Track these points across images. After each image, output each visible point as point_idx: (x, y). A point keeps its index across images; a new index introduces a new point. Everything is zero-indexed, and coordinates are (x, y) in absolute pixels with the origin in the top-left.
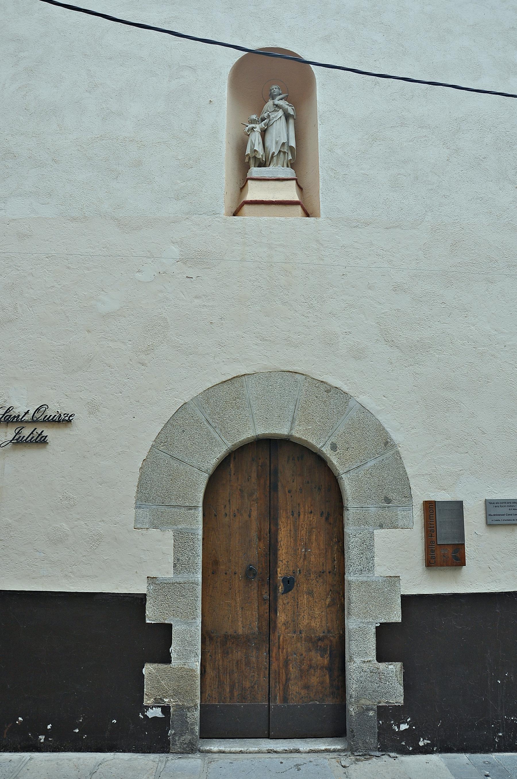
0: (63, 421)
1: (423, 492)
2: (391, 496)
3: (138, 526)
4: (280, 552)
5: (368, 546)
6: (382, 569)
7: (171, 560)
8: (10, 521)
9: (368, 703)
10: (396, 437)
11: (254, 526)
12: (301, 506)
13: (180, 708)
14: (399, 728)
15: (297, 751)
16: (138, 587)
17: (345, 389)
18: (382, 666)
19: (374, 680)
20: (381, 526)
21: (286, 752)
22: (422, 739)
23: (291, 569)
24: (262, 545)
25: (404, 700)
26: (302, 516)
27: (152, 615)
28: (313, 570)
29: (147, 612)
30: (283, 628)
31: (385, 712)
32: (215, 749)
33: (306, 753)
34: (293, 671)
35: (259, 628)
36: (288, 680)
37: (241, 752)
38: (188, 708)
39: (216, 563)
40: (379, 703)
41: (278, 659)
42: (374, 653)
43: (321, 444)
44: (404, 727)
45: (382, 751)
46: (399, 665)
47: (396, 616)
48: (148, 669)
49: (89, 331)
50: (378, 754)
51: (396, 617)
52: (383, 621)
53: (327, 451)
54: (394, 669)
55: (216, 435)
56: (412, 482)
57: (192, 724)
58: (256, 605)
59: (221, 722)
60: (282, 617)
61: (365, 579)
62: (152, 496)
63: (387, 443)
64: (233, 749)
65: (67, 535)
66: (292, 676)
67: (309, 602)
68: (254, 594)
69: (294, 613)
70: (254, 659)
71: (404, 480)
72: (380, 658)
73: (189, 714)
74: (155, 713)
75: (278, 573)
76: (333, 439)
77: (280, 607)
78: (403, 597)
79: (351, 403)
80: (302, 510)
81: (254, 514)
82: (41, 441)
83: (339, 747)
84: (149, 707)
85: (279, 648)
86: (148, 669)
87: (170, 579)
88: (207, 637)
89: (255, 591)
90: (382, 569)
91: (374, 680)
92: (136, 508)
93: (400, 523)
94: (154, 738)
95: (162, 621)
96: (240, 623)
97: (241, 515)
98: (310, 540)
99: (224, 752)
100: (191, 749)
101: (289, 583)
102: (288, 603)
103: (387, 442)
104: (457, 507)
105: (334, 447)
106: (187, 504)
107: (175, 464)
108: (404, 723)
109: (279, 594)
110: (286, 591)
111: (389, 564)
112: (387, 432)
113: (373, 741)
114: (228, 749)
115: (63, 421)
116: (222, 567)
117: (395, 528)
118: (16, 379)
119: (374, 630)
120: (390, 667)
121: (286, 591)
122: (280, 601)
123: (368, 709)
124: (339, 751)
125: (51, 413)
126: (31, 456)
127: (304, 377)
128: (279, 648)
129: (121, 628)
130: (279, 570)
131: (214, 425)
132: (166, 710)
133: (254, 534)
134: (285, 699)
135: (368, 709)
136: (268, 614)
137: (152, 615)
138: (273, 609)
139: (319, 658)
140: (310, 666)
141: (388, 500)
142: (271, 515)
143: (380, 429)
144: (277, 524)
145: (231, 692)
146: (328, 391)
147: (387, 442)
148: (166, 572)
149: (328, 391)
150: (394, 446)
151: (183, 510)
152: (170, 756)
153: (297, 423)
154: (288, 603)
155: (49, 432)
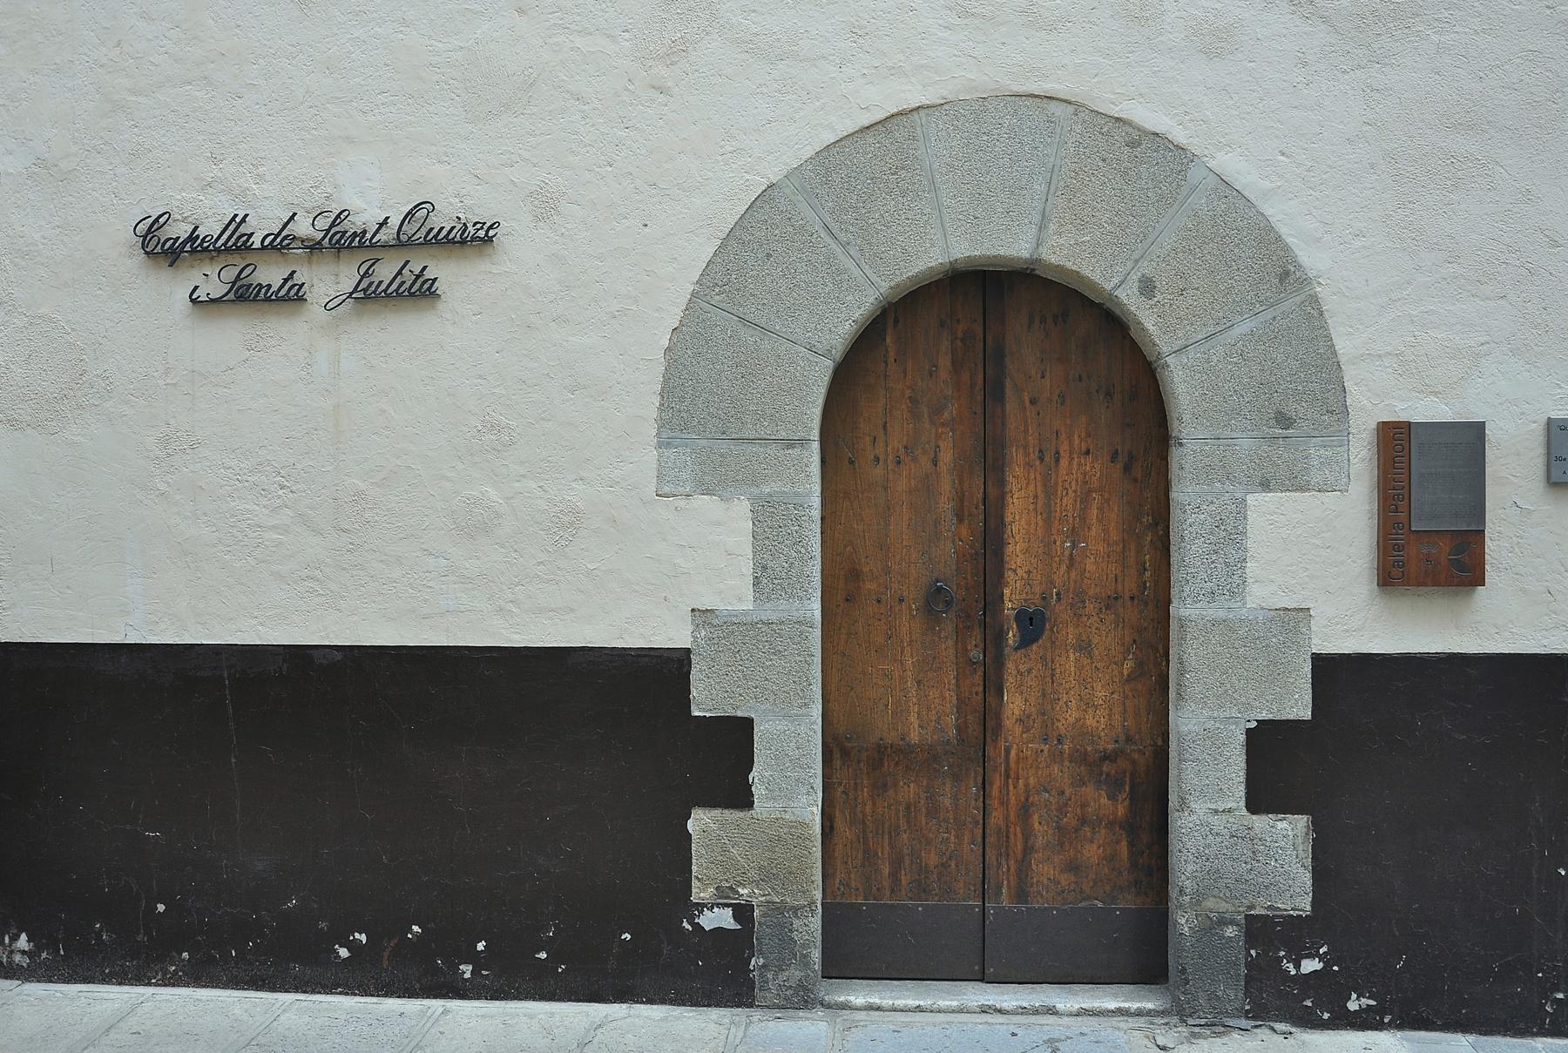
0: (472, 240)
1: (1377, 396)
2: (1291, 409)
3: (667, 489)
4: (1009, 549)
5: (1232, 534)
6: (1265, 590)
7: (747, 568)
8: (362, 486)
9: (1223, 906)
10: (1311, 259)
11: (946, 485)
12: (1063, 436)
13: (776, 909)
14: (1298, 966)
15: (1052, 1011)
16: (671, 634)
17: (1179, 136)
18: (1260, 822)
19: (1240, 851)
20: (1265, 486)
21: (1023, 1011)
22: (1354, 996)
23: (1038, 590)
24: (964, 531)
25: (1313, 903)
26: (1064, 463)
27: (706, 699)
28: (1091, 593)
29: (694, 692)
30: (1018, 729)
31: (1268, 934)
32: (858, 1000)
33: (1071, 1015)
34: (1042, 831)
35: (959, 729)
36: (1028, 850)
37: (919, 1009)
38: (795, 910)
39: (855, 575)
40: (1252, 907)
41: (1004, 803)
42: (1241, 791)
43: (1116, 281)
44: (1310, 966)
45: (1254, 1018)
46: (1302, 821)
47: (1299, 707)
48: (700, 822)
49: (521, 11)
50: (1244, 1023)
51: (1299, 707)
52: (1264, 716)
53: (1129, 298)
54: (1289, 832)
55: (850, 264)
56: (1350, 375)
57: (804, 946)
58: (952, 675)
59: (868, 944)
60: (1014, 704)
61: (1221, 614)
62: (698, 416)
63: (1287, 273)
64: (900, 1003)
65: (498, 515)
66: (1040, 842)
67: (1080, 669)
68: (947, 649)
69: (1044, 695)
70: (947, 802)
71: (1328, 369)
72: (1256, 804)
73: (796, 923)
74: (718, 919)
75: (1006, 599)
76: (1146, 268)
77: (1010, 681)
78: (1318, 660)
79: (1195, 174)
80: (1064, 448)
81: (947, 456)
82: (422, 292)
83: (1150, 1006)
84: (704, 905)
85: (1008, 776)
86: (700, 822)
87: (745, 613)
88: (835, 748)
89: (950, 643)
90: (1265, 590)
91: (1240, 851)
92: (660, 445)
93: (1316, 478)
94: (719, 972)
95: (730, 712)
96: (913, 718)
97: (915, 459)
98: (1083, 519)
99: (878, 1009)
100: (802, 1000)
101: (1032, 624)
102: (1029, 671)
103: (1287, 273)
104: (1468, 441)
105: (1147, 287)
106: (783, 434)
107: (749, 336)
108: (1310, 956)
109: (1007, 651)
110: (1026, 641)
111: (1286, 575)
112: (1286, 248)
113: (1233, 994)
114: (887, 1003)
115: (472, 240)
116: (870, 586)
117: (1301, 489)
118: (349, 140)
119: (1242, 738)
120: (1280, 825)
121: (1026, 641)
122: (1010, 666)
123: (1223, 922)
124: (1149, 1013)
125: (442, 220)
126: (398, 336)
127: (1071, 109)
128: (1008, 776)
129: (631, 725)
130: (1007, 591)
131: (843, 237)
132: (743, 912)
133: (946, 505)
134: (1021, 895)
135: (1223, 922)
136: (981, 696)
137: (706, 699)
138: (993, 685)
139: (1104, 801)
140: (1083, 820)
141: (1284, 420)
142: (989, 459)
143: (1268, 237)
144: (1002, 482)
145: (894, 875)
146: (1133, 144)
147: (1287, 273)
148: (733, 593)
149: (1133, 144)
150: (1305, 281)
151: (772, 450)
152: (756, 1014)
153: (1052, 227)
154: (1029, 671)
155: (444, 271)
